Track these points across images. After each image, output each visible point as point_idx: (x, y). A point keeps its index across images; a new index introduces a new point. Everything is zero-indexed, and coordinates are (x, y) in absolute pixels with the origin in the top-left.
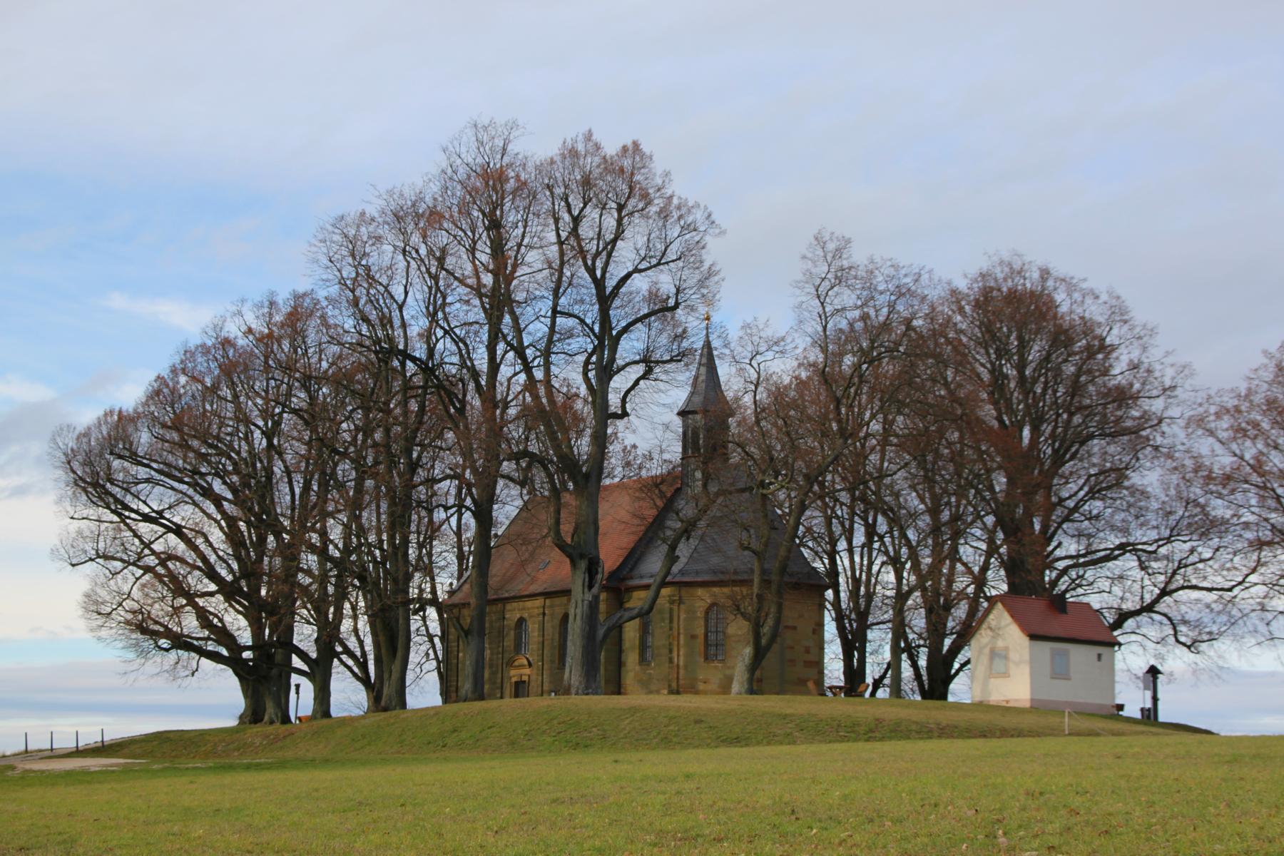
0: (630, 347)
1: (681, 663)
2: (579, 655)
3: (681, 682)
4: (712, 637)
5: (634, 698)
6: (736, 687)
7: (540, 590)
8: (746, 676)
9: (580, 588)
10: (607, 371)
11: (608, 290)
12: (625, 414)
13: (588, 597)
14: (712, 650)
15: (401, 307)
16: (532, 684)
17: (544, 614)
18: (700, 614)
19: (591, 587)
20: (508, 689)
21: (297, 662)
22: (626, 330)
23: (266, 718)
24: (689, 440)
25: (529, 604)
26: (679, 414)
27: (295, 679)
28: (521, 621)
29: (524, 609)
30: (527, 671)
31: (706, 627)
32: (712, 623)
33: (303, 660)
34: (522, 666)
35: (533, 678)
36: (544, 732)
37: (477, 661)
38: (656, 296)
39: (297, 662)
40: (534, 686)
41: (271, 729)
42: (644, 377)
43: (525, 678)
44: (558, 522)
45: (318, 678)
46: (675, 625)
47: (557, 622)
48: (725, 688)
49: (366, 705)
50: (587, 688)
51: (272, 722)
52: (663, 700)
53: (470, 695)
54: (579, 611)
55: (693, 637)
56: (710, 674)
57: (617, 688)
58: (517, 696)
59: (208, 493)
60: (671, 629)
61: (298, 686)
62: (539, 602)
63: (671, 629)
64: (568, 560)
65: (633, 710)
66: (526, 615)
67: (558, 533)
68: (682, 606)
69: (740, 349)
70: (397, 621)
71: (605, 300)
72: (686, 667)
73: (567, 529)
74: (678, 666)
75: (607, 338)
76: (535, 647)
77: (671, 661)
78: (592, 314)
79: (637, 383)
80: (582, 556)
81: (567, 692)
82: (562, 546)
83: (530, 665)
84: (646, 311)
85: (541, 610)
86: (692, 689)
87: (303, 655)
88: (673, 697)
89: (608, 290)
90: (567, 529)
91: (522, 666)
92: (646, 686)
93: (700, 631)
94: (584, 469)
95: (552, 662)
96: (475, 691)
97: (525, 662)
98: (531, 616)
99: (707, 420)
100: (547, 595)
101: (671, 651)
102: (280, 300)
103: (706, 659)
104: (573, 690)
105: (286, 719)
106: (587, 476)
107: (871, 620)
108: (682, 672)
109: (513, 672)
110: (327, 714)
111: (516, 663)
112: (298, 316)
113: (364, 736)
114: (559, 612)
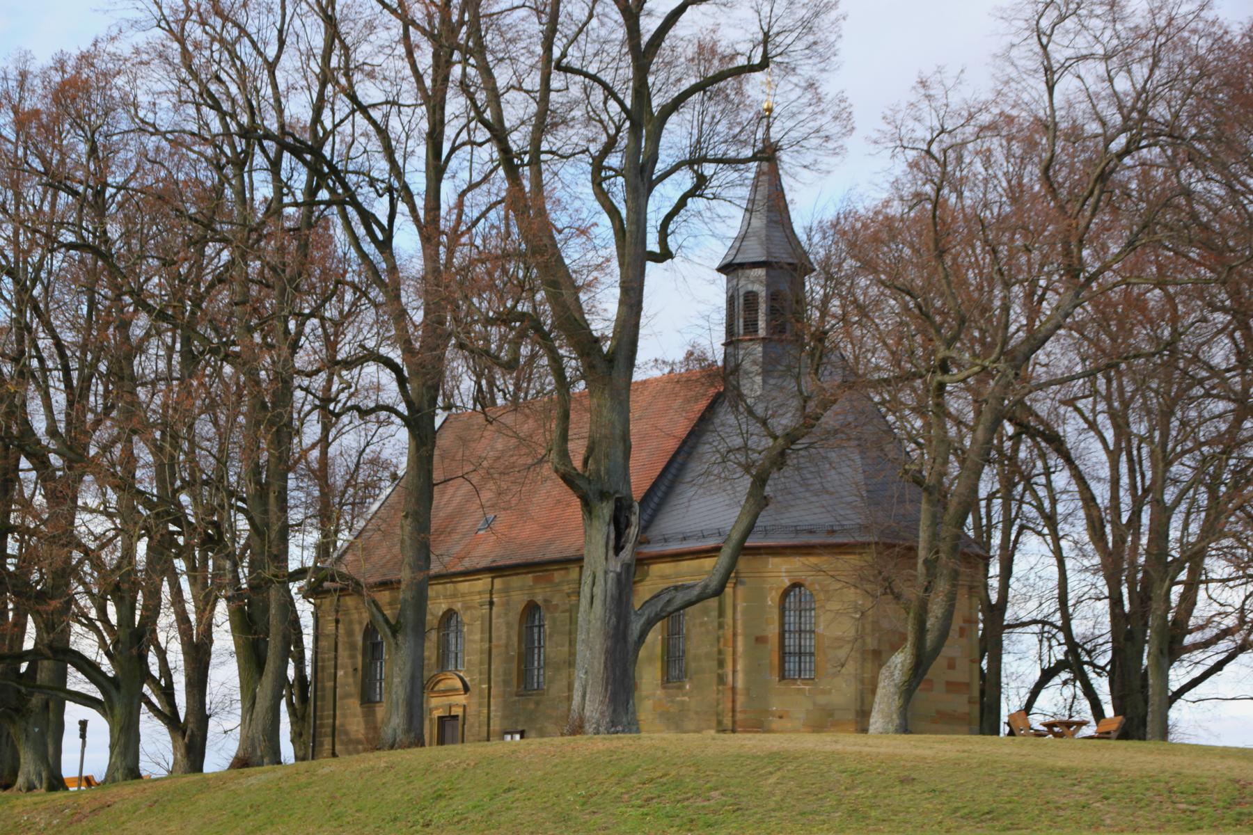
0: (676, 137)
1: (740, 684)
2: (598, 665)
3: (739, 716)
4: (791, 642)
5: (654, 738)
6: (877, 721)
7: (484, 563)
8: (897, 703)
9: (602, 550)
10: (642, 178)
11: (645, 39)
12: (665, 255)
13: (616, 565)
14: (791, 665)
15: (271, 67)
16: (470, 720)
17: (491, 603)
18: (772, 600)
19: (618, 549)
20: (430, 730)
21: (76, 681)
22: (675, 105)
23: (21, 780)
24: (740, 312)
25: (464, 586)
26: (723, 269)
27: (73, 713)
28: (450, 614)
29: (454, 596)
30: (461, 699)
31: (782, 624)
32: (791, 618)
33: (93, 680)
34: (451, 691)
35: (472, 710)
36: (618, 799)
37: (413, 679)
38: (713, 52)
39: (76, 681)
40: (474, 723)
41: (30, 799)
42: (694, 192)
43: (455, 711)
44: (564, 437)
45: (118, 710)
46: (728, 620)
47: (514, 616)
48: (861, 721)
49: (171, 759)
50: (614, 723)
51: (30, 788)
52: (709, 743)
53: (400, 736)
54: (598, 591)
55: (761, 640)
56: (793, 702)
57: (632, 726)
58: (441, 741)
59: (91, 292)
60: (721, 626)
61: (83, 724)
62: (483, 583)
63: (721, 626)
64: (577, 502)
65: (779, 759)
66: (458, 606)
67: (564, 455)
68: (740, 589)
69: (911, 124)
70: (266, 609)
71: (643, 55)
72: (747, 690)
73: (577, 450)
74: (734, 689)
75: (645, 120)
76: (475, 658)
77: (721, 679)
78: (621, 74)
79: (682, 203)
80: (603, 496)
81: (577, 729)
82: (569, 479)
83: (466, 689)
84: (693, 81)
85: (486, 597)
86: (758, 726)
87: (89, 668)
88: (728, 736)
89: (645, 39)
90: (577, 450)
91: (451, 691)
92: (675, 721)
93: (773, 631)
94: (605, 349)
95: (506, 683)
96: (408, 731)
97: (459, 685)
98: (468, 608)
99: (772, 285)
100: (496, 571)
101: (721, 664)
102: (35, 67)
103: (783, 677)
104: (589, 728)
105: (56, 782)
106: (610, 359)
107: (1009, 616)
108: (740, 699)
109: (434, 702)
110: (133, 773)
111: (441, 686)
112: (78, 93)
113: (256, 808)
114: (519, 600)
